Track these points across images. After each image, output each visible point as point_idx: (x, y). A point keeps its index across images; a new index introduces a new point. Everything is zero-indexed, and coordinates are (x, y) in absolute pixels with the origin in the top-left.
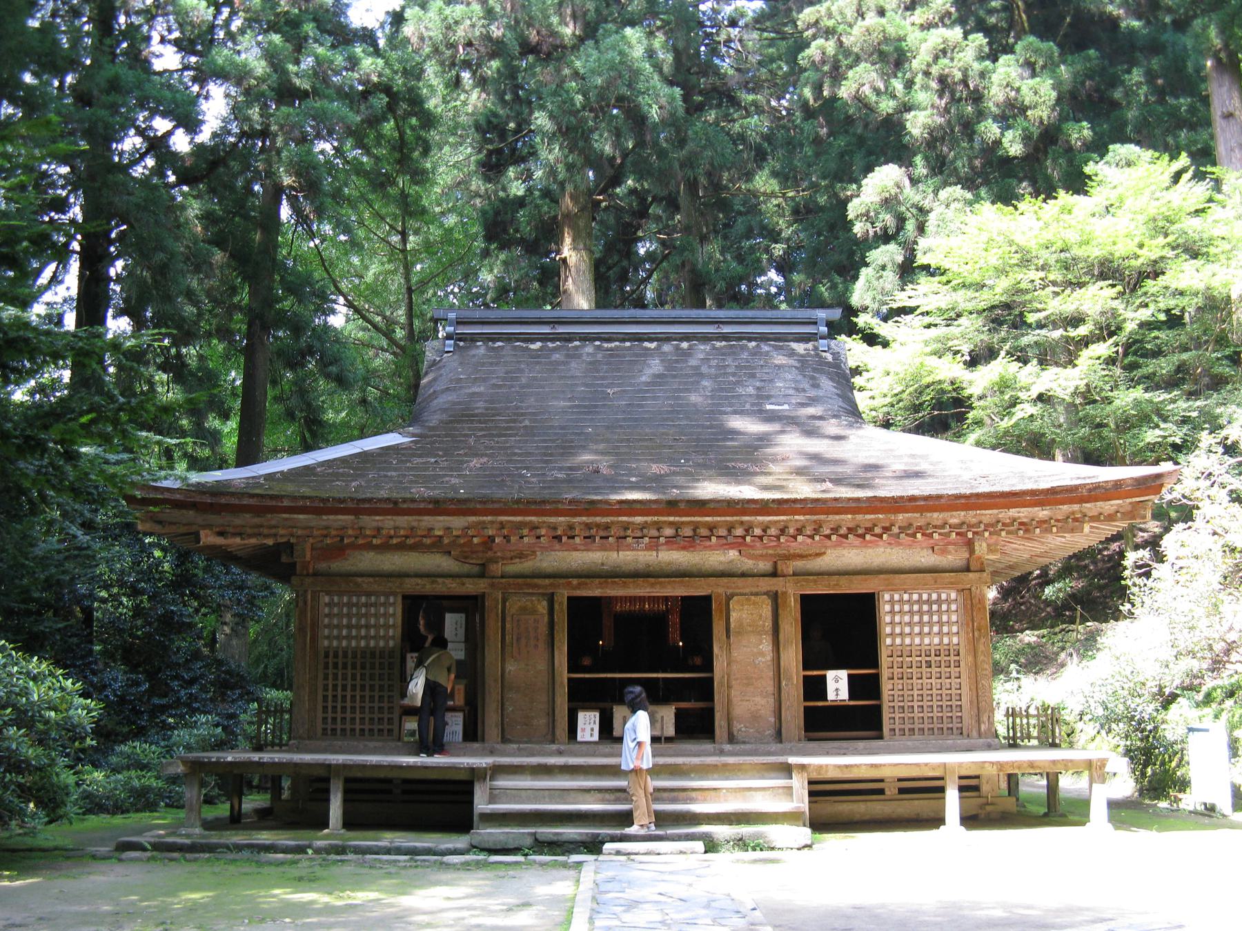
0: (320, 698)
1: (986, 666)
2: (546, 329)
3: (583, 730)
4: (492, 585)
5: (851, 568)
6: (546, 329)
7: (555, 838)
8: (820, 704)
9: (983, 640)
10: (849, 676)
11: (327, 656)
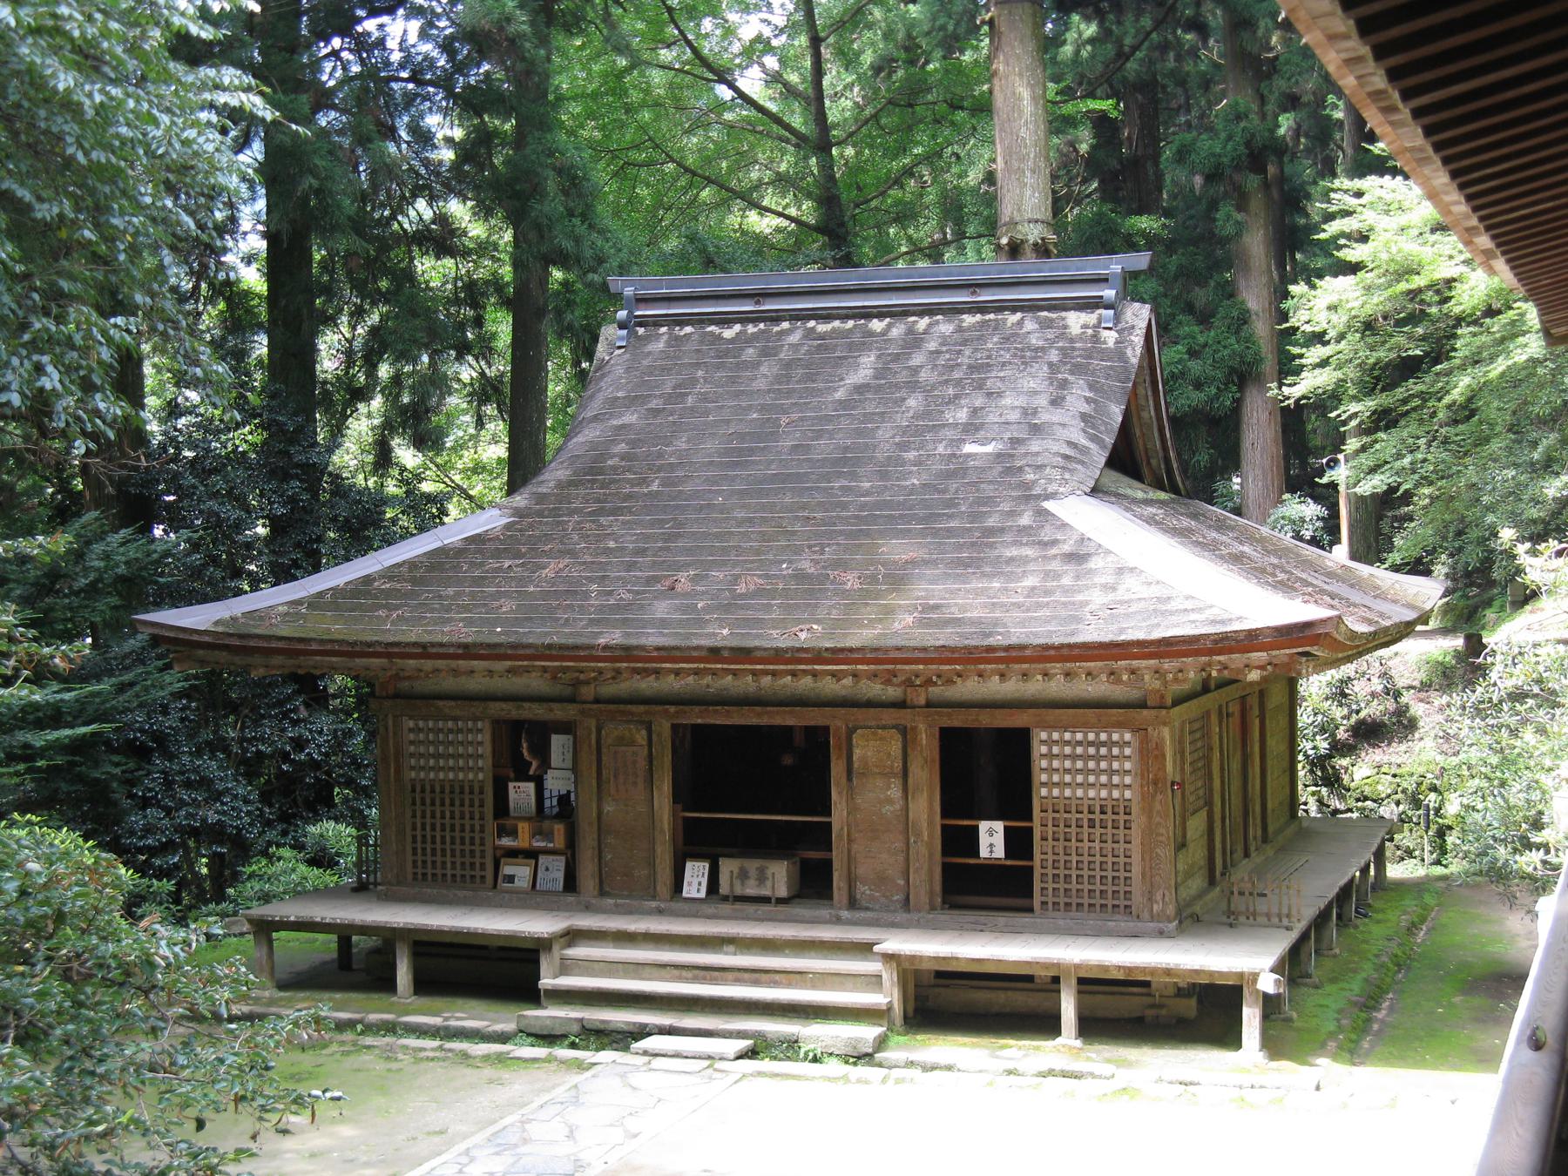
0: (409, 839)
1: (1162, 831)
2: (748, 307)
3: (690, 884)
4: (582, 712)
5: (999, 697)
6: (748, 307)
7: (602, 1027)
8: (972, 861)
9: (1159, 797)
10: (1006, 828)
11: (414, 790)
